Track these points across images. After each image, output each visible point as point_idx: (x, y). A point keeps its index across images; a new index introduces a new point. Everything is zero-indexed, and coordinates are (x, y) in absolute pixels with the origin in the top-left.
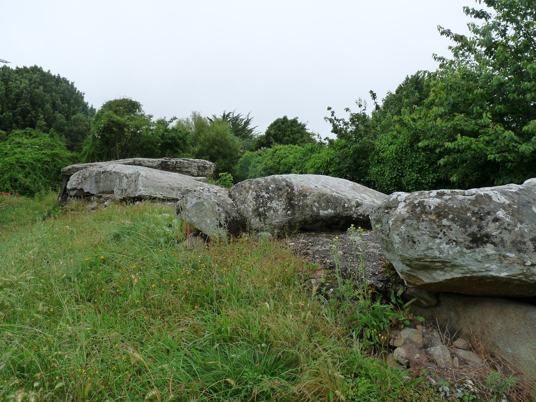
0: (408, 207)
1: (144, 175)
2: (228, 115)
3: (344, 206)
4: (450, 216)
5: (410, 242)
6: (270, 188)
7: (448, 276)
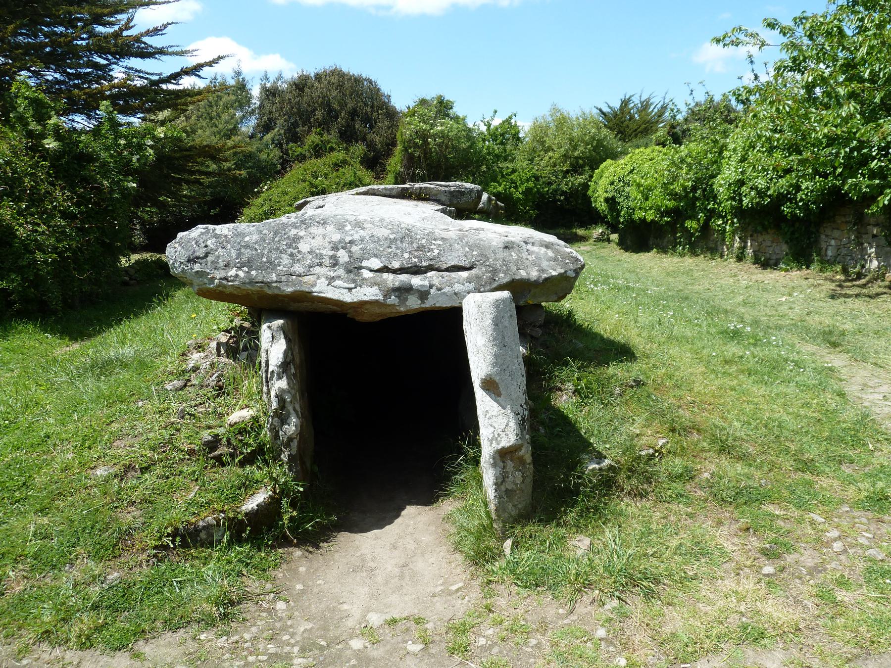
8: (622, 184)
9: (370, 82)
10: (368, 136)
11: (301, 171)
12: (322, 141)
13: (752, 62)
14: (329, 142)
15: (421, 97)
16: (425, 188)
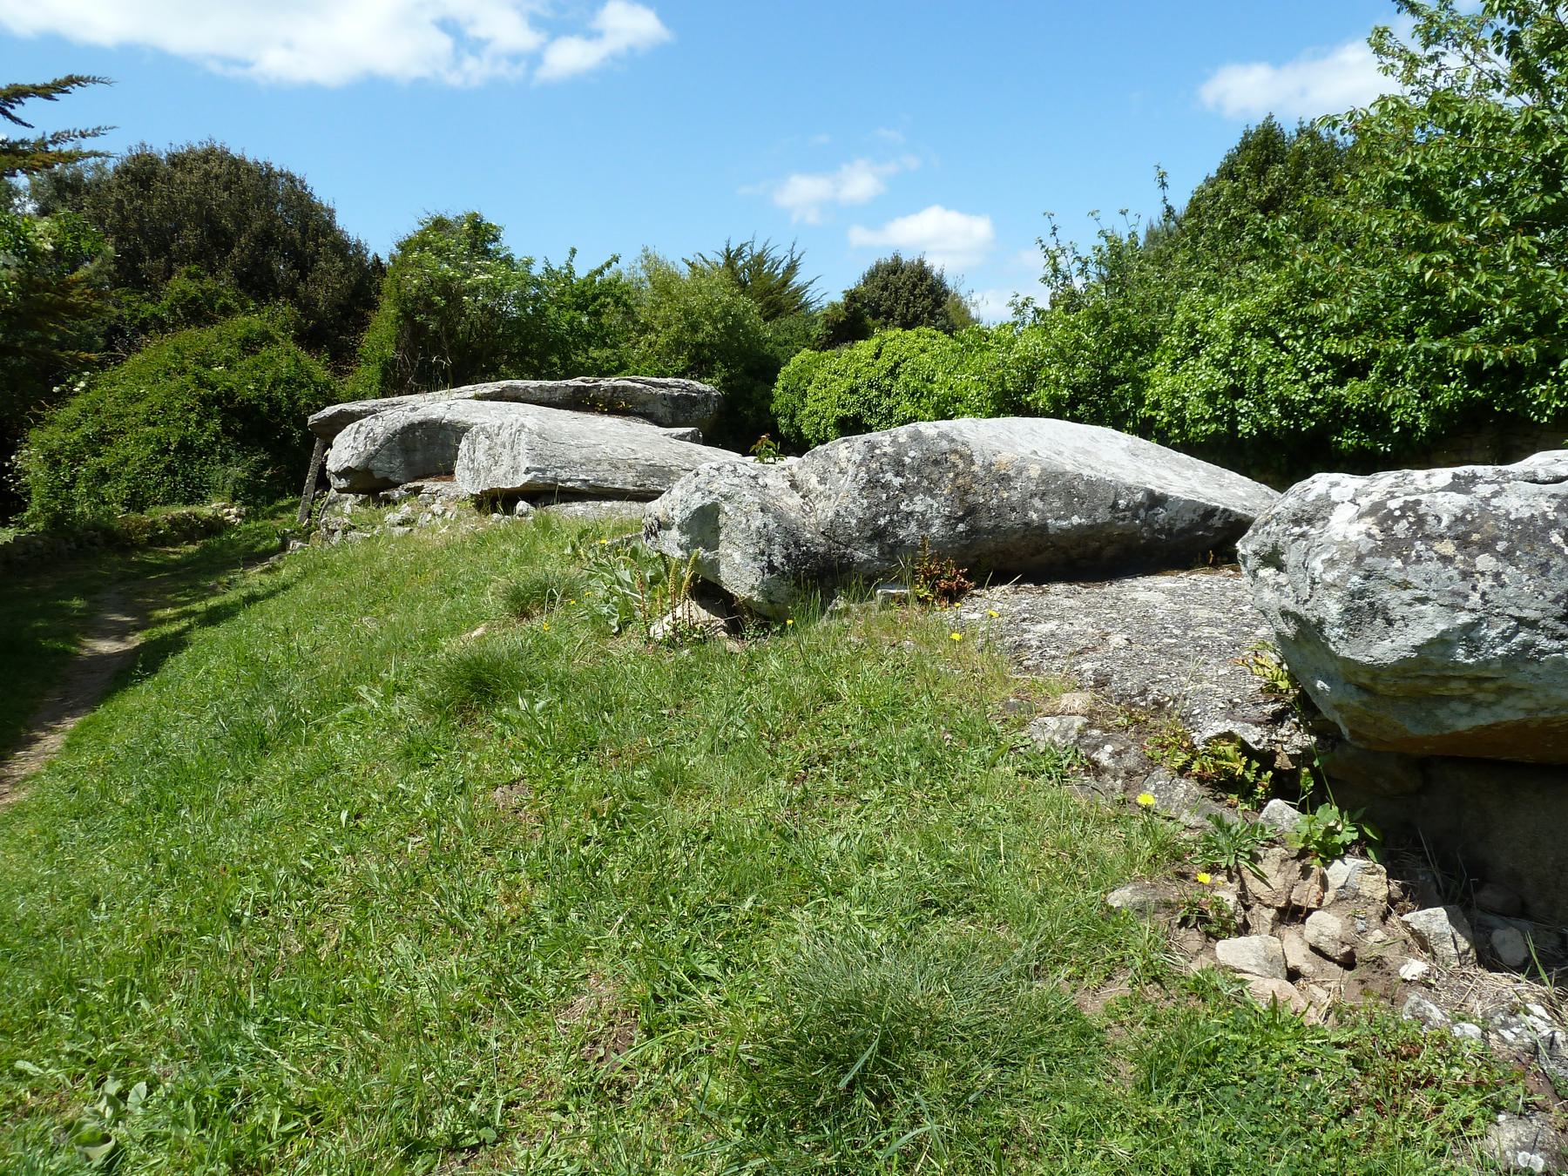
0: (1370, 520)
1: (535, 428)
2: (739, 252)
3: (1114, 506)
4: (1501, 546)
5: (1379, 621)
6: (907, 460)
7: (1484, 718)
8: (875, 393)
9: (291, 179)
10: (301, 287)
11: (168, 352)
12: (203, 292)
13: (1164, 185)
14: (219, 295)
15: (435, 215)
16: (510, 387)
